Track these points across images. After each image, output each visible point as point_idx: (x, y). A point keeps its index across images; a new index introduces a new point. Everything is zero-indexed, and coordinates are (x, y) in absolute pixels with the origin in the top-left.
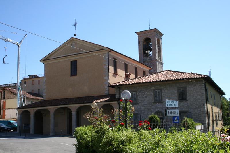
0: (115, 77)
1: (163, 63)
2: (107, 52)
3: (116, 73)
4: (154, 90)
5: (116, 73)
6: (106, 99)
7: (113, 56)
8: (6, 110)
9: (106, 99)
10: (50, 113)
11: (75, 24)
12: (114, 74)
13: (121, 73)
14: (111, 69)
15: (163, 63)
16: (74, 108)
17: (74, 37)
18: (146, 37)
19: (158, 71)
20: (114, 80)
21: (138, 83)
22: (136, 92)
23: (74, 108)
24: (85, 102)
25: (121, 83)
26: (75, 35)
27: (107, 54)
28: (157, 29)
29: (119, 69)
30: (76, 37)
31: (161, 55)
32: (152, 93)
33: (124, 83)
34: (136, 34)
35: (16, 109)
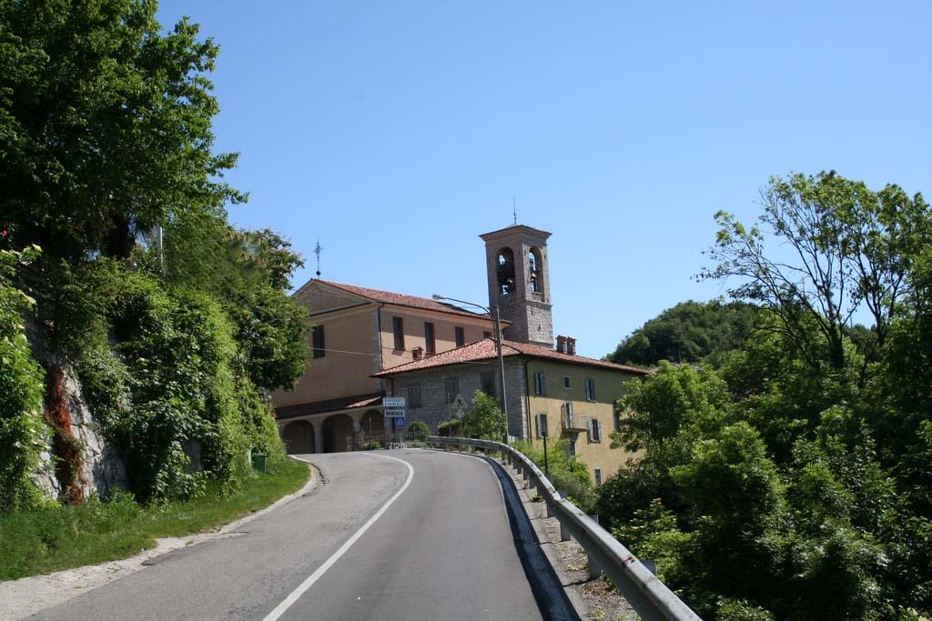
0: (400, 355)
1: (551, 306)
2: (375, 309)
3: (400, 347)
4: (446, 379)
5: (400, 347)
6: (371, 401)
7: (392, 313)
8: (544, 331)
9: (371, 401)
10: (352, 420)
11: (318, 250)
12: (396, 349)
13: (414, 341)
14: (388, 339)
15: (551, 306)
16: (316, 420)
17: (316, 277)
18: (508, 246)
19: (437, 352)
20: (392, 362)
21: (413, 370)
22: (419, 384)
23: (316, 420)
24: (294, 414)
25: (394, 370)
26: (318, 273)
27: (376, 313)
28: (526, 225)
29: (407, 334)
30: (322, 278)
31: (545, 286)
32: (443, 385)
33: (410, 367)
34: (480, 239)
35: (841, 261)
